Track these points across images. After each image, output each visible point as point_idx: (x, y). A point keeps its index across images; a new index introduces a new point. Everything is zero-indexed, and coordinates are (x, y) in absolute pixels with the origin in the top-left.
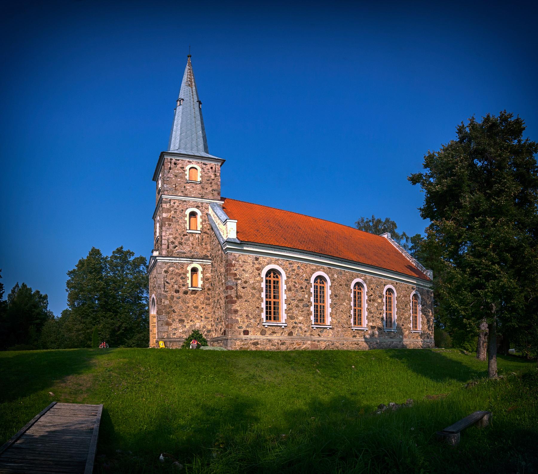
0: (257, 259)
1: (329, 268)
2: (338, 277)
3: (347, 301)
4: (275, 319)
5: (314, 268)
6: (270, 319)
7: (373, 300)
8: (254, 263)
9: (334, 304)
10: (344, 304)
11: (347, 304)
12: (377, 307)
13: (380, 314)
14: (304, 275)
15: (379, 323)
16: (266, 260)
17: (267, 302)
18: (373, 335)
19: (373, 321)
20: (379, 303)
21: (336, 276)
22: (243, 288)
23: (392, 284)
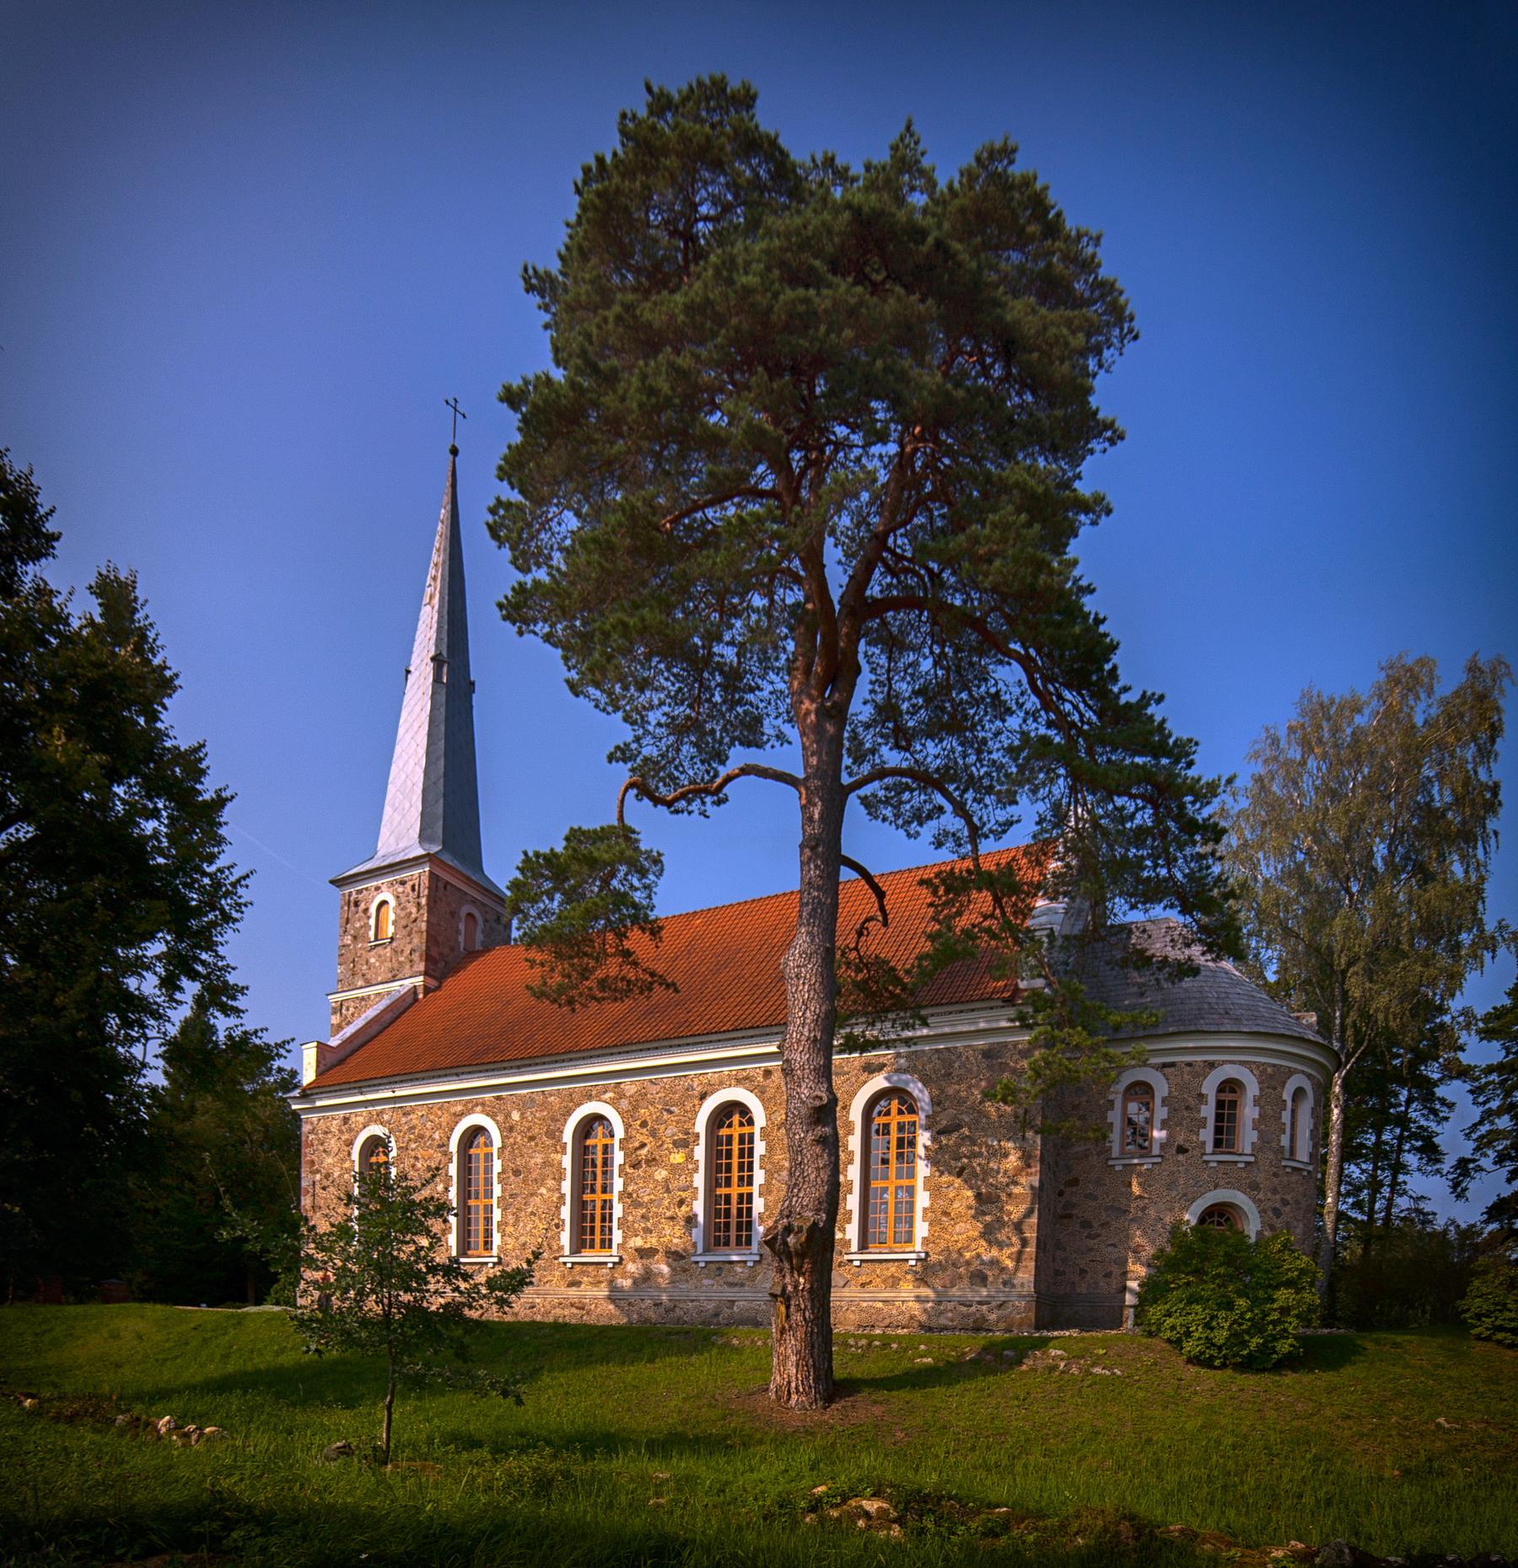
0: (346, 1120)
1: (498, 1098)
2: (523, 1116)
3: (550, 1183)
4: (739, 1243)
5: (459, 1108)
6: (727, 1244)
7: (648, 1162)
8: (340, 1131)
9: (511, 1196)
10: (543, 1190)
11: (549, 1190)
12: (666, 1180)
13: (681, 1203)
14: (437, 1136)
15: (674, 1236)
16: (360, 1119)
17: (750, 1183)
18: (647, 1277)
19: (648, 1231)
20: (675, 1169)
21: (516, 1116)
22: (324, 1188)
23: (740, 1081)
